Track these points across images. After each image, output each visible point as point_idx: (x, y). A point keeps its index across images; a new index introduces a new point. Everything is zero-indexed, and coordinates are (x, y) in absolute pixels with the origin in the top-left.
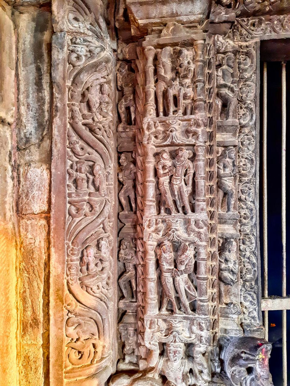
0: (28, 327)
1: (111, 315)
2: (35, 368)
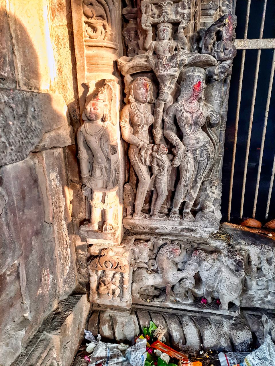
0: (55, 12)
1: (116, 12)
2: (64, 44)
